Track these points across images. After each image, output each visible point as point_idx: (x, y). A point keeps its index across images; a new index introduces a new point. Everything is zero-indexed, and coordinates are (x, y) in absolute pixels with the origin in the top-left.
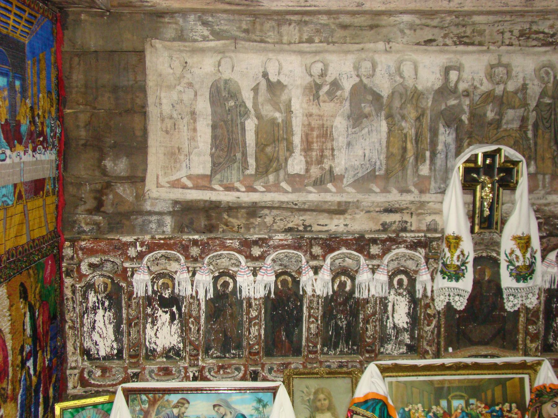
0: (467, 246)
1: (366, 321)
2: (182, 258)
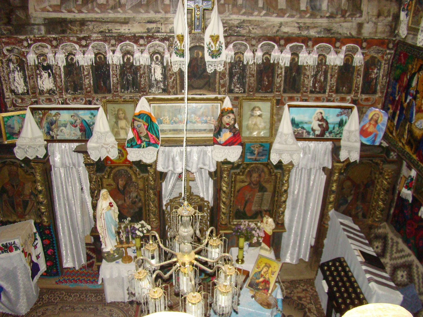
2: (49, 47)
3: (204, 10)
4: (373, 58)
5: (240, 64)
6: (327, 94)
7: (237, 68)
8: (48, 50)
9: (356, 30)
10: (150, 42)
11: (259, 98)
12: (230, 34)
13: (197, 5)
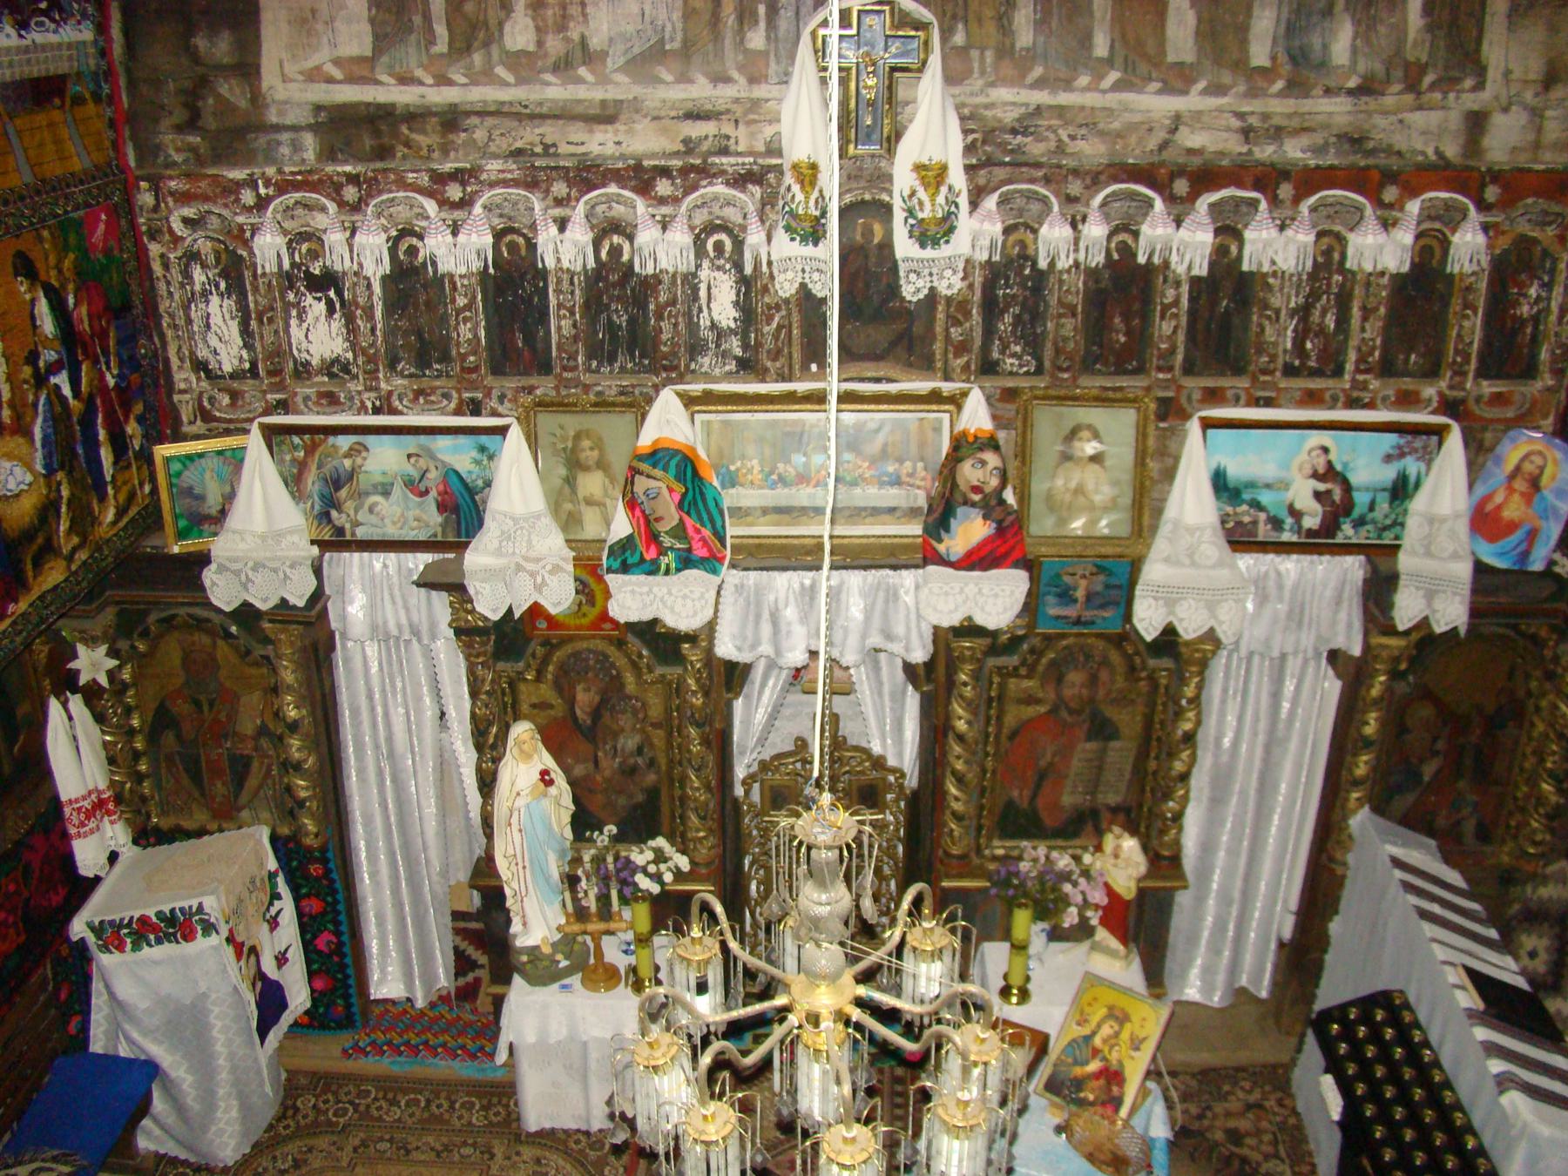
0: (831, 181)
1: (659, 316)
2: (332, 207)
3: (894, 69)
4: (1524, 244)
5: (1022, 267)
6: (1347, 377)
7: (1011, 284)
8: (327, 220)
9: (1461, 141)
10: (695, 188)
11: (1095, 392)
12: (988, 159)
13: (868, 54)
